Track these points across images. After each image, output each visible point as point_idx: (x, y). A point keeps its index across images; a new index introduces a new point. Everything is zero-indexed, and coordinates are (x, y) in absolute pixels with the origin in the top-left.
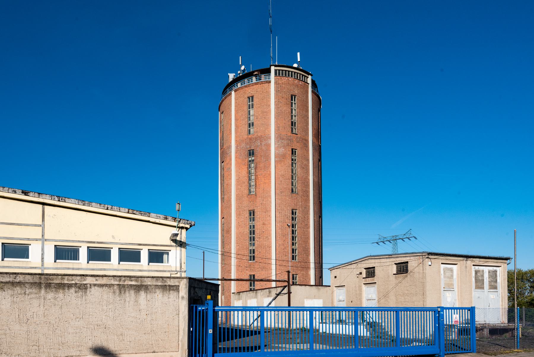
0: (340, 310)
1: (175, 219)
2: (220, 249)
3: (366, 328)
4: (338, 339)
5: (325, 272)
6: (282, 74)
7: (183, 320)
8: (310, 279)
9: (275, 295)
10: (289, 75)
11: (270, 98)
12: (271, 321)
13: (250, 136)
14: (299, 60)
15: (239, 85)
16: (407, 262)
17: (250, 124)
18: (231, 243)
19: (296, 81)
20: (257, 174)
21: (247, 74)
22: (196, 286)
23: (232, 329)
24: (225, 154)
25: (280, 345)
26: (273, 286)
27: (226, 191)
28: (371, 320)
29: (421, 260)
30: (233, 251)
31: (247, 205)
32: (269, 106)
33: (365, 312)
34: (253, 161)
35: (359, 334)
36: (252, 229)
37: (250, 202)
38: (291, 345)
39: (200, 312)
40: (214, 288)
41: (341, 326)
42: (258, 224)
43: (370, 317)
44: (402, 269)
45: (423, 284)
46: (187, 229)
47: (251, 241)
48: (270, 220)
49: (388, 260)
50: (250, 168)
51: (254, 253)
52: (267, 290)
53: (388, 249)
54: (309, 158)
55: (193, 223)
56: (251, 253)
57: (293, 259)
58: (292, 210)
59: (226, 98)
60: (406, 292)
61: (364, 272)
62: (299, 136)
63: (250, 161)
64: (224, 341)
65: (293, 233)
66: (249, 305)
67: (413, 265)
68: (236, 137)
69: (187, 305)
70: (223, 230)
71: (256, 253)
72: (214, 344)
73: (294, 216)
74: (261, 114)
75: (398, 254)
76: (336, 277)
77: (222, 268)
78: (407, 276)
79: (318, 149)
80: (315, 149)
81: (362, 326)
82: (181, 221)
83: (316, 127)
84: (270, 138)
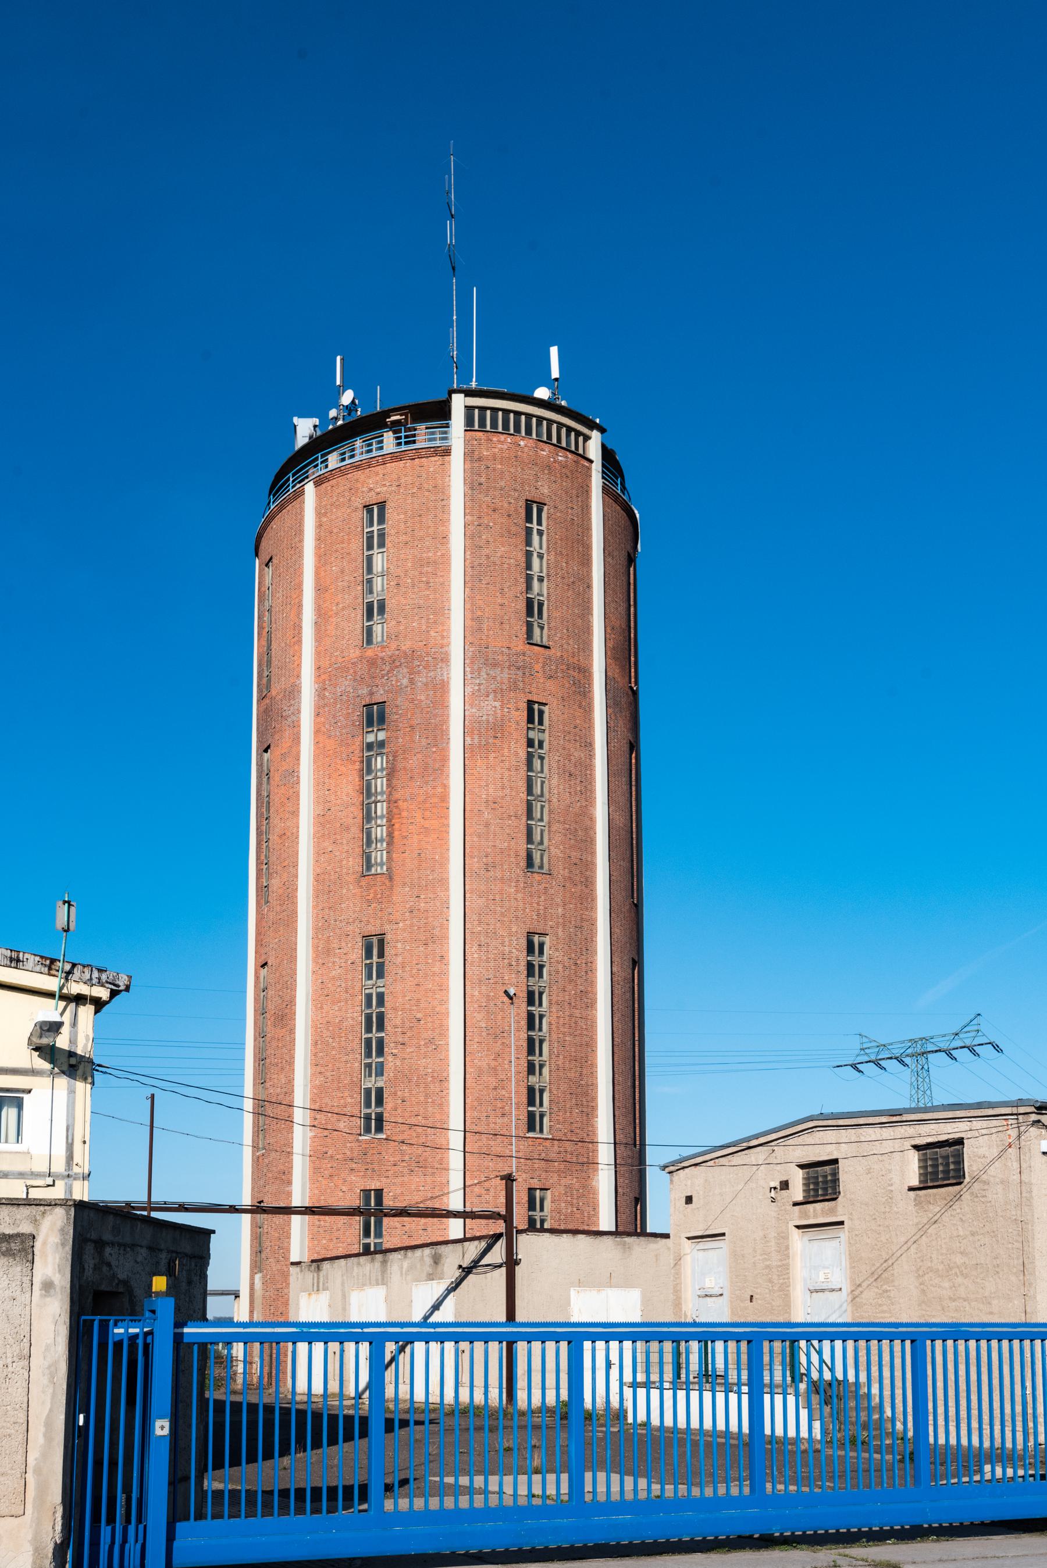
0: (707, 1335)
1: (50, 965)
2: (249, 1090)
3: (809, 1407)
4: (695, 1453)
5: (654, 1178)
6: (494, 424)
7: (45, 1381)
8: (595, 1208)
9: (458, 1273)
10: (517, 429)
11: (445, 509)
12: (430, 1377)
13: (370, 653)
14: (555, 373)
15: (333, 460)
16: (960, 1142)
17: (370, 606)
18: (291, 1063)
19: (546, 451)
20: (396, 795)
21: (361, 419)
22: (107, 1237)
23: (285, 1412)
24: (277, 717)
25: (464, 1481)
26: (452, 1237)
27: (276, 862)
28: (827, 1376)
29: (1014, 1133)
30: (301, 1095)
31: (357, 917)
32: (445, 538)
33: (803, 1344)
34: (381, 744)
35: (768, 1431)
36: (375, 1010)
37: (369, 903)
38: (508, 1479)
39: (118, 1345)
40: (186, 1247)
41: (707, 1396)
42: (397, 988)
43: (822, 1361)
44: (943, 1167)
45: (1023, 1227)
46: (99, 1004)
47: (369, 1055)
48: (445, 973)
49: (887, 1132)
50: (369, 771)
51: (380, 1102)
52: (427, 1251)
53: (892, 1088)
54: (592, 736)
55: (122, 982)
56: (368, 1105)
57: (531, 1127)
58: (530, 935)
59: (281, 507)
60: (959, 1259)
61: (797, 1179)
62: (555, 652)
63: (370, 746)
64: (235, 1462)
65: (531, 1026)
66: (354, 1318)
67: (982, 1151)
68: (318, 654)
69: (65, 1318)
70: (261, 1012)
71: (389, 1103)
72: (177, 1480)
73: (535, 960)
74: (415, 569)
75: (926, 1110)
76: (689, 1200)
77: (257, 1161)
78: (959, 1197)
79: (627, 704)
80: (616, 704)
81: (791, 1399)
82: (77, 972)
83: (619, 623)
84: (445, 659)
